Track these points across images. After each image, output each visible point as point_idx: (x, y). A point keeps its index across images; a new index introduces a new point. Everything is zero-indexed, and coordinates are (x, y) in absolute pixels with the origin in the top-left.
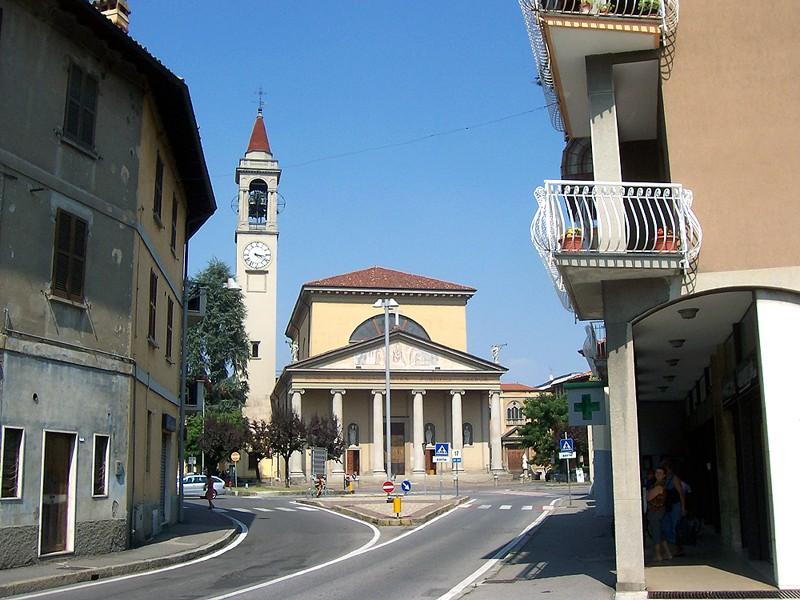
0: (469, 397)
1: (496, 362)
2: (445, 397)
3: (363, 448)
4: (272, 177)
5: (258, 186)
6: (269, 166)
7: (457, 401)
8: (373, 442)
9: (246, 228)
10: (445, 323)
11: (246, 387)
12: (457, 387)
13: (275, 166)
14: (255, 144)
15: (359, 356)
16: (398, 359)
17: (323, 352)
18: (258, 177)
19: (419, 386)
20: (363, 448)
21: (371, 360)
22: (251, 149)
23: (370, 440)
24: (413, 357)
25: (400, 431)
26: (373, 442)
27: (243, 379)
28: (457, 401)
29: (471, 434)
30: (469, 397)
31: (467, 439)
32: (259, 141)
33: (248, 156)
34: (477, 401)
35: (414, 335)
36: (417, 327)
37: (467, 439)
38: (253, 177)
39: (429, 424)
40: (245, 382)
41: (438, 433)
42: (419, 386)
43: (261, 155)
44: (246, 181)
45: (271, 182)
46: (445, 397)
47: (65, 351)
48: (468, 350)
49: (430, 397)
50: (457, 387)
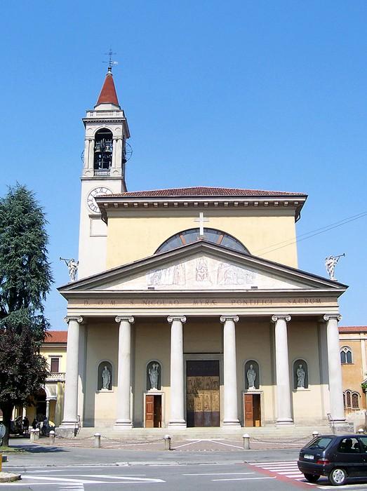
0: (296, 323)
1: (332, 279)
2: (266, 324)
3: (265, 391)
4: (116, 126)
5: (104, 137)
6: (115, 115)
7: (281, 330)
8: (117, 386)
9: (91, 175)
10: (270, 237)
11: (44, 325)
12: (281, 312)
13: (120, 115)
14: (103, 97)
15: (152, 275)
16: (203, 278)
17: (87, 276)
18: (104, 126)
19: (229, 312)
20: (265, 391)
21: (165, 280)
22: (99, 103)
23: (273, 382)
24: (222, 274)
25: (203, 370)
26: (117, 386)
27: (38, 313)
28: (281, 330)
29: (159, 377)
30: (296, 323)
31: (301, 381)
32: (109, 94)
33: (97, 109)
34: (308, 329)
35: (240, 256)
36: (233, 243)
37: (301, 381)
38: (97, 127)
39: (156, 363)
40: (42, 317)
41: (255, 369)
42: (229, 312)
43: (109, 107)
44: (91, 131)
45: (117, 131)
46: (266, 324)
47: (159, 307)
48: (299, 267)
49: (244, 324)
50: (281, 312)
